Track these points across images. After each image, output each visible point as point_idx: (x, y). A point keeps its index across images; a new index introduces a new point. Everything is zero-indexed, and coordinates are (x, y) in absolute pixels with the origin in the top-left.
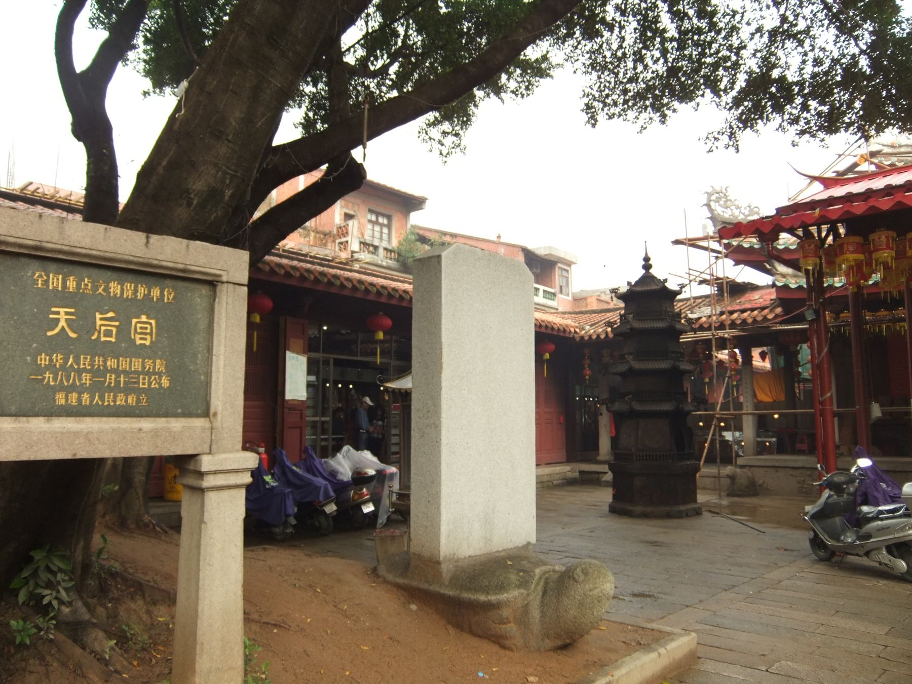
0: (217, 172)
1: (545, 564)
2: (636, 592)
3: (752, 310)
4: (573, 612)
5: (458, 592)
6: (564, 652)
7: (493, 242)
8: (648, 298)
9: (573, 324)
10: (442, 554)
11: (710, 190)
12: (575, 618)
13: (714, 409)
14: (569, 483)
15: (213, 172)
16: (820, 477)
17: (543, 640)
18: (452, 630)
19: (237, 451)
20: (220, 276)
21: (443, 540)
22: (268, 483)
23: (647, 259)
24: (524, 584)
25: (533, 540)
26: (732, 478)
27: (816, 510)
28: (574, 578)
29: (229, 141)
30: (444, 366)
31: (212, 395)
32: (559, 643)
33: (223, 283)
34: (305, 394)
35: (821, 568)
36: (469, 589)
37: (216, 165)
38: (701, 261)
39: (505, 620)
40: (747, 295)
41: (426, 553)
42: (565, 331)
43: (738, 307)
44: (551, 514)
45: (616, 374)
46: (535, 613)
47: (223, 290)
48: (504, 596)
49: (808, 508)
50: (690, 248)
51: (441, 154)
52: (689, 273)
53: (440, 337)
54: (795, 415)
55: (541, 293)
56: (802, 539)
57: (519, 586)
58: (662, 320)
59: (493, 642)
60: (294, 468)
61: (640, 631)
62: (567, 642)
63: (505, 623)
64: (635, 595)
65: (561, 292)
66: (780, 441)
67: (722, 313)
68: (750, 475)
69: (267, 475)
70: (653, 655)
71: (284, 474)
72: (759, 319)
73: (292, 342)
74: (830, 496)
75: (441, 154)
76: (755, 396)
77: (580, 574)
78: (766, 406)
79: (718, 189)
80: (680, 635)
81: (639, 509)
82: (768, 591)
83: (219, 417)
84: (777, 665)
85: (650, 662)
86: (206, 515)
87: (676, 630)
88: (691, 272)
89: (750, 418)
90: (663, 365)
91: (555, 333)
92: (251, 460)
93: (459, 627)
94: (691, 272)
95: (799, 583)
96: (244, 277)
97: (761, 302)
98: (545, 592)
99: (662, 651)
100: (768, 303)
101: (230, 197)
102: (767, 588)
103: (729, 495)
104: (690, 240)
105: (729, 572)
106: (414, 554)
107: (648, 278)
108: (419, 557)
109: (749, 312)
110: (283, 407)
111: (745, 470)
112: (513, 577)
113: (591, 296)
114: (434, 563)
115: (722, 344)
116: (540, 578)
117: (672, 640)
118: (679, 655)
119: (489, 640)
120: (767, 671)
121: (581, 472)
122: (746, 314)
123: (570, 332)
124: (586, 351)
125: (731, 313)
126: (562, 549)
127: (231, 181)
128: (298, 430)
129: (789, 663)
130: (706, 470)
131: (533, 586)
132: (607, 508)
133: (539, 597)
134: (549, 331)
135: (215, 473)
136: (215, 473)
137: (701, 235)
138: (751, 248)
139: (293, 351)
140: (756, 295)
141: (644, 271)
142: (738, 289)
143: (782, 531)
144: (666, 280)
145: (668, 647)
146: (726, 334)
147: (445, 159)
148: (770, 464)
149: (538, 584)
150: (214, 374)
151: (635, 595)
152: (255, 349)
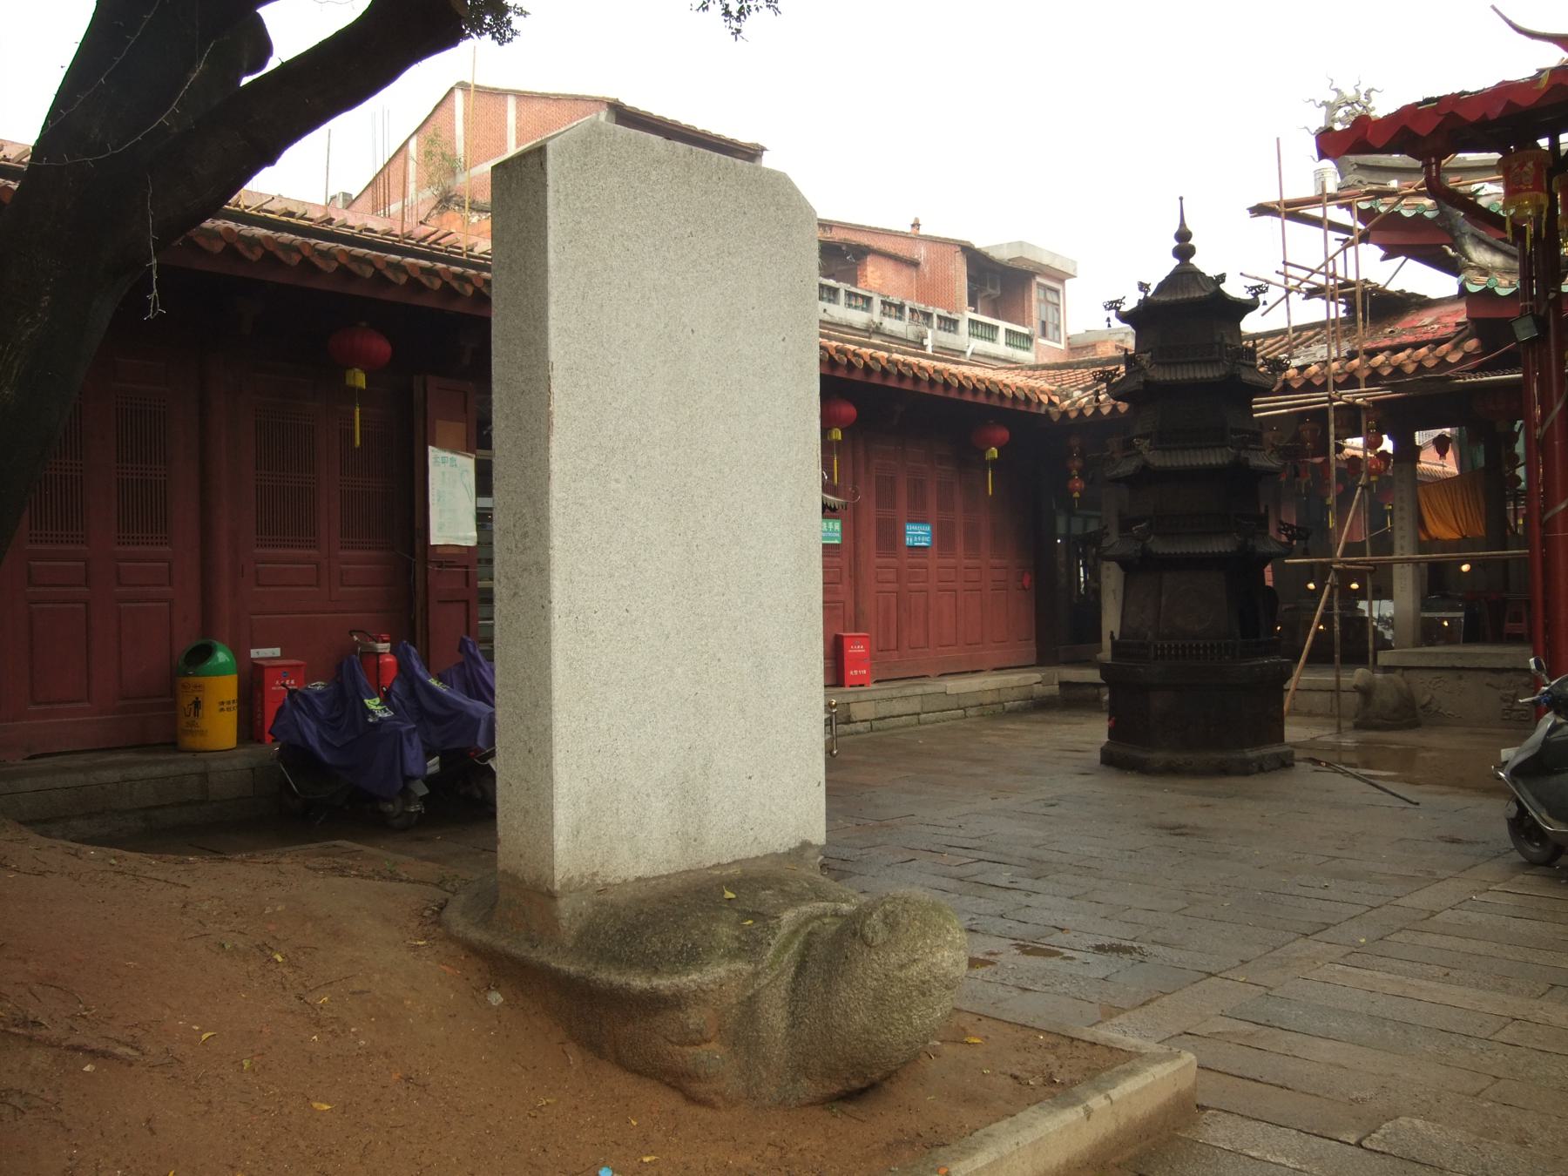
1: (821, 897)
2: (1106, 941)
3: (1416, 346)
4: (861, 1018)
5: (591, 965)
6: (850, 1108)
7: (904, 235)
8: (1187, 316)
9: (1046, 387)
11: (1332, 97)
13: (1329, 552)
14: (1039, 706)
16: (1538, 683)
17: (795, 1080)
18: (574, 1056)
21: (561, 842)
22: (372, 712)
23: (1183, 236)
24: (748, 947)
25: (819, 836)
26: (1366, 692)
27: (1521, 758)
28: (863, 936)
30: (557, 421)
32: (836, 1088)
34: (474, 534)
35: (1530, 883)
36: (616, 960)
38: (1308, 246)
39: (695, 1036)
40: (1408, 319)
42: (1028, 400)
43: (1387, 342)
44: (981, 770)
45: (1117, 480)
46: (775, 1018)
48: (691, 979)
49: (1507, 754)
50: (1288, 223)
51: (727, 13)
52: (1284, 278)
53: (546, 350)
54: (1505, 562)
55: (1001, 335)
56: (1493, 816)
57: (732, 955)
58: (1216, 362)
59: (668, 1084)
60: (433, 682)
61: (1064, 1049)
62: (859, 1084)
63: (693, 1043)
64: (1100, 949)
65: (1044, 334)
66: (1472, 619)
67: (1352, 355)
68: (1404, 685)
70: (1072, 1115)
71: (412, 694)
72: (1430, 363)
73: (441, 427)
74: (1555, 728)
75: (727, 13)
76: (1421, 523)
77: (880, 926)
78: (1446, 545)
79: (1350, 93)
80: (1157, 1059)
81: (1159, 757)
82: (1401, 937)
84: (1387, 1127)
85: (1063, 1129)
87: (1150, 1047)
88: (1291, 270)
89: (1408, 570)
90: (1215, 458)
91: (1008, 405)
93: (594, 1046)
94: (1291, 270)
95: (1475, 917)
97: (1437, 330)
98: (801, 967)
99: (1097, 1102)
100: (1450, 331)
102: (1400, 931)
103: (1358, 727)
104: (1288, 204)
105: (1322, 893)
106: (504, 872)
107: (1184, 274)
108: (515, 880)
109: (1408, 351)
110: (426, 562)
111: (1395, 676)
112: (725, 932)
113: (1105, 342)
114: (542, 894)
115: (1352, 420)
116: (795, 933)
117: (1131, 1073)
118: (1144, 1108)
119: (660, 1080)
120: (1359, 1145)
121: (1064, 685)
122: (1402, 356)
123: (1040, 402)
124: (1075, 442)
125: (1372, 353)
126: (976, 843)
128: (463, 605)
129: (1418, 1123)
130: (1301, 677)
131: (770, 953)
132: (1097, 756)
133: (787, 978)
134: (995, 402)
137: (1310, 192)
138: (1419, 217)
139: (443, 447)
140: (1427, 318)
141: (1177, 262)
142: (1386, 306)
143: (1457, 800)
144: (1222, 278)
145: (1115, 1094)
146: (1359, 396)
147: (735, 24)
148: (1446, 663)
149: (785, 947)
151: (1100, 949)
152: (358, 442)
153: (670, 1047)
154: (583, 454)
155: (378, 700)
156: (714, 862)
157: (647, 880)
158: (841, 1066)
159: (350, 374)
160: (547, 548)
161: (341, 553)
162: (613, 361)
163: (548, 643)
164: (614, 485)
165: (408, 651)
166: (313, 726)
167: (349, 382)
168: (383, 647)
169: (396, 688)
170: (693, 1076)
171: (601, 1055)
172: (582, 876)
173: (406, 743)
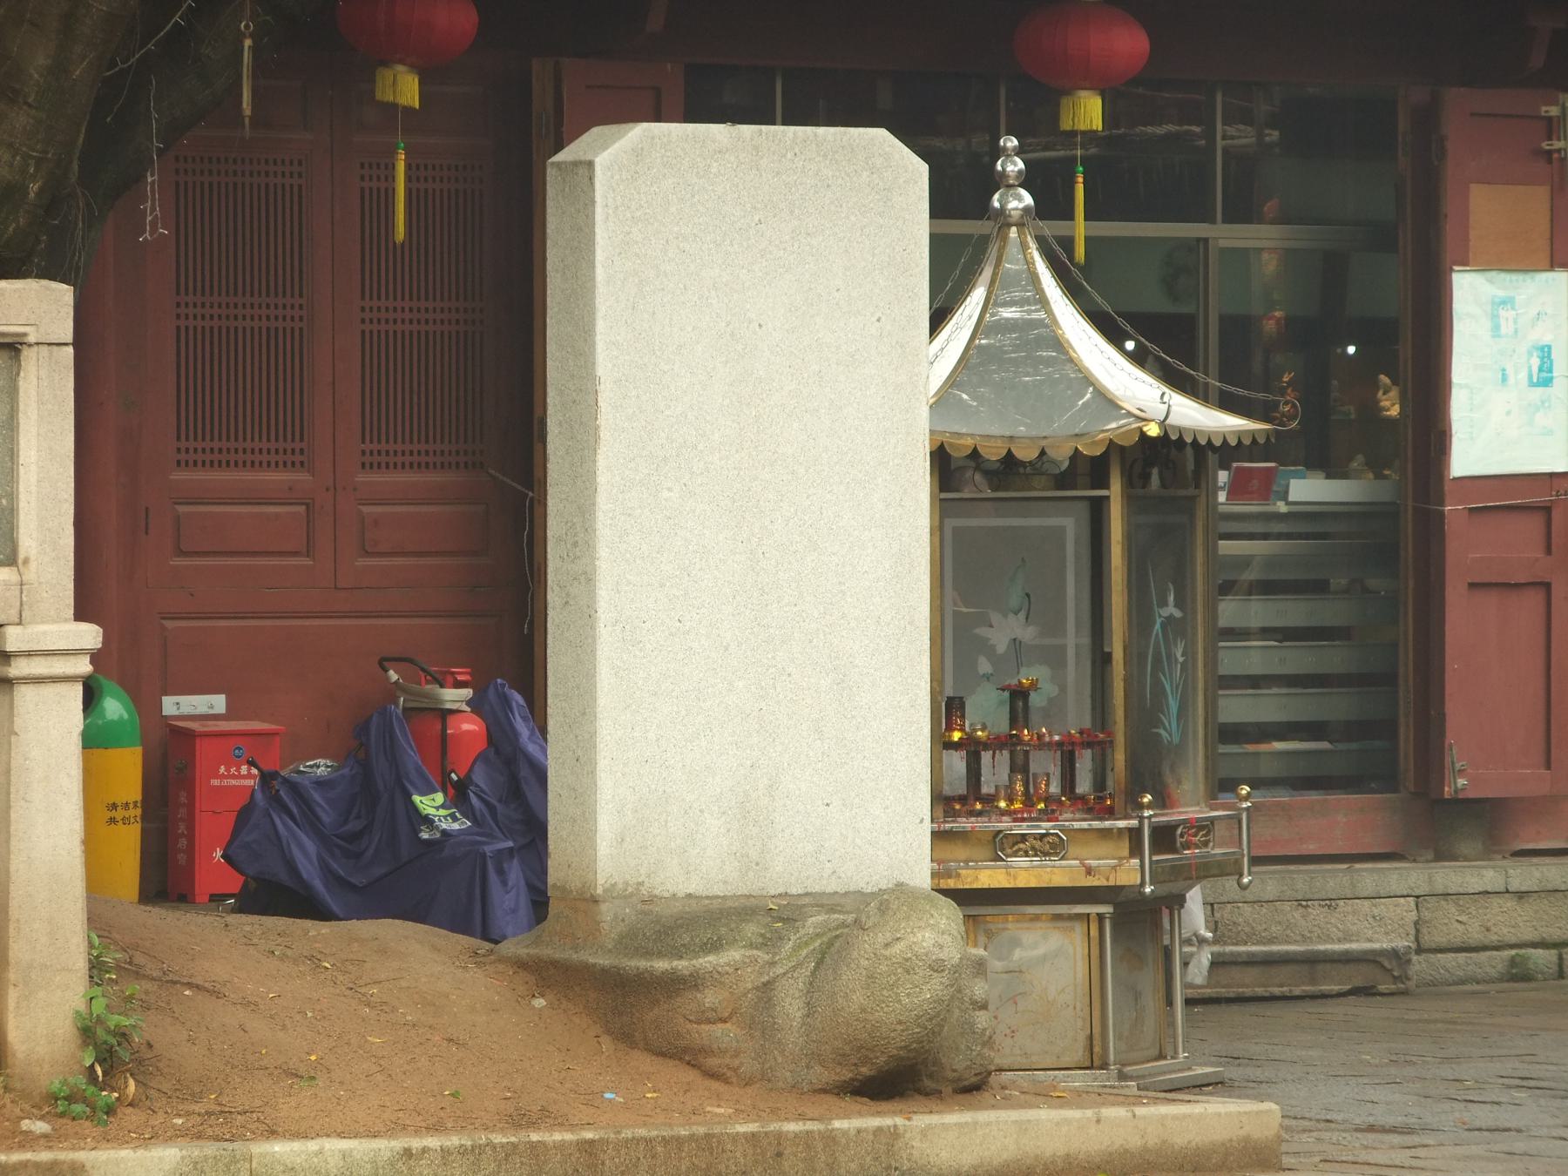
0: (14, 157)
4: (858, 998)
10: (601, 881)
12: (863, 1010)
15: (7, 157)
18: (607, 1044)
19: (66, 620)
20: (25, 335)
22: (428, 821)
29: (30, 106)
31: (21, 531)
33: (30, 345)
36: (648, 954)
37: (11, 145)
39: (710, 1015)
41: (575, 884)
47: (29, 357)
63: (709, 1022)
69: (428, 790)
83: (33, 565)
86: (18, 722)
92: (90, 635)
93: (627, 1038)
96: (66, 331)
101: (37, 194)
127: (36, 170)
135: (29, 654)
136: (29, 654)
145: (1140, 1111)
150: (22, 496)
153: (689, 1026)
154: (632, 465)
155: (439, 798)
156: (781, 890)
157: (699, 898)
158: (847, 1048)
159: (384, 76)
160: (593, 559)
161: (362, 478)
162: (666, 368)
163: (593, 652)
164: (666, 494)
165: (505, 701)
166: (311, 846)
167: (384, 94)
168: (454, 697)
169: (479, 777)
170: (706, 1051)
171: (633, 1045)
172: (626, 883)
173: (493, 877)
